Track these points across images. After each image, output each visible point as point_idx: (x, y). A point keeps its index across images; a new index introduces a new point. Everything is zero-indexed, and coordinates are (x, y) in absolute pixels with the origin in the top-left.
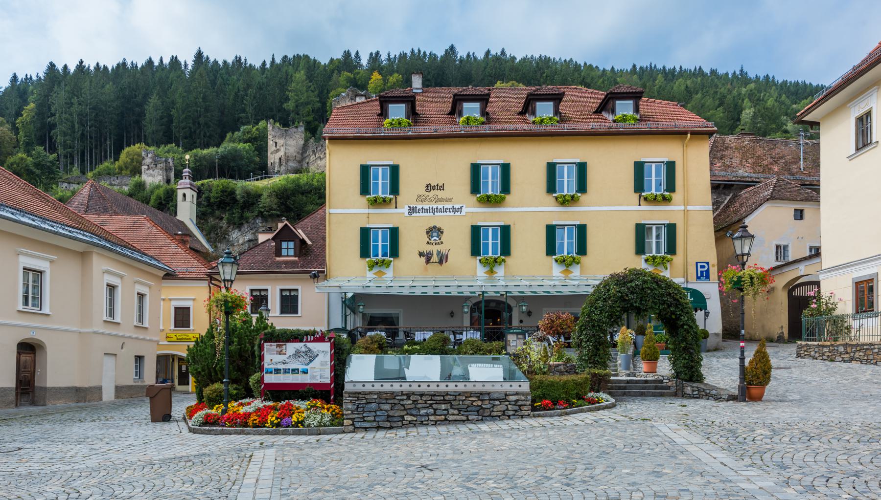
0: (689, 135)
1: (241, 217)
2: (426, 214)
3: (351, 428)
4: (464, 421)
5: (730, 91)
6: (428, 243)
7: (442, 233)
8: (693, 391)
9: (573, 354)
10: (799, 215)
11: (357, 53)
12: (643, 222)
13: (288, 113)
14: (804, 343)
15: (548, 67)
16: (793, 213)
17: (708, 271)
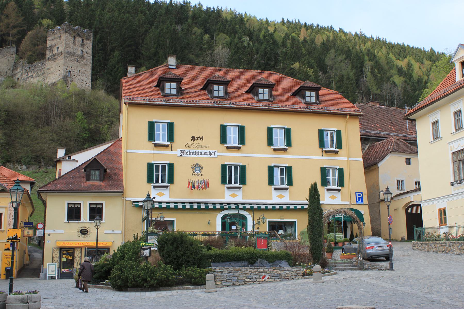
0: (348, 116)
2: (192, 156)
3: (221, 285)
4: (273, 281)
6: (193, 174)
7: (202, 168)
8: (369, 267)
10: (408, 162)
12: (324, 166)
14: (415, 242)
16: (405, 160)
17: (362, 198)
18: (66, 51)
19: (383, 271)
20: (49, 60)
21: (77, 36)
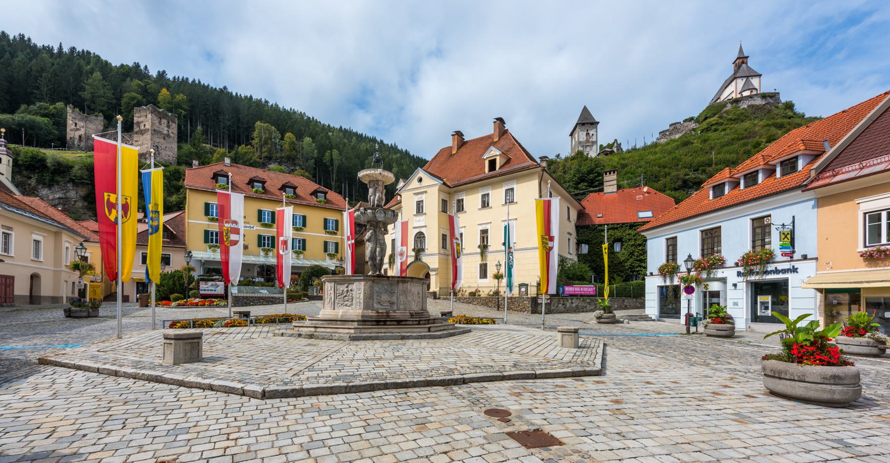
1: (52, 180)
5: (388, 156)
9: (298, 288)
10: (587, 122)
11: (146, 67)
13: (84, 100)
15: (290, 118)
18: (244, 187)
19: (796, 249)
20: (136, 133)
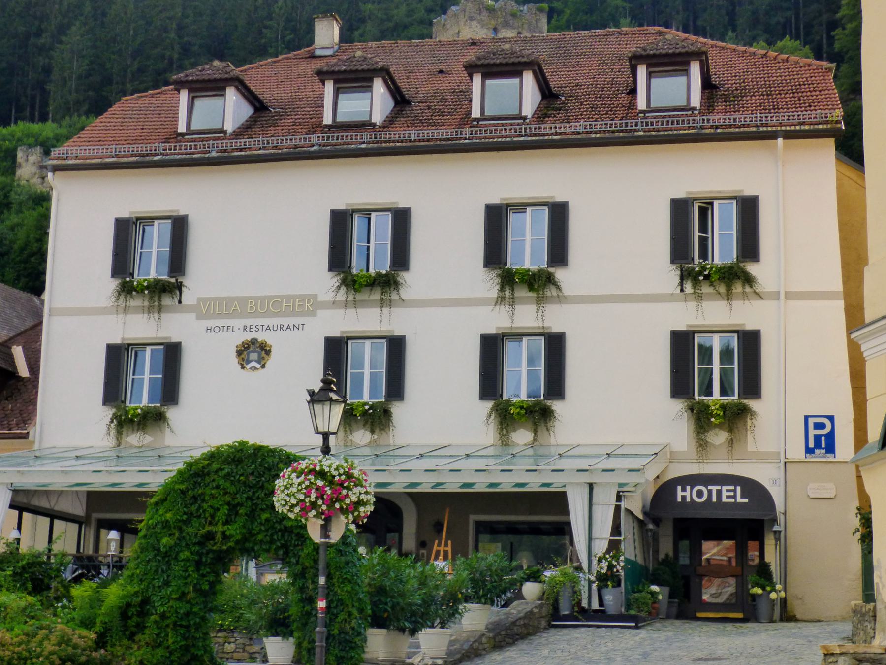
7: (268, 353)
21: (503, 27)
